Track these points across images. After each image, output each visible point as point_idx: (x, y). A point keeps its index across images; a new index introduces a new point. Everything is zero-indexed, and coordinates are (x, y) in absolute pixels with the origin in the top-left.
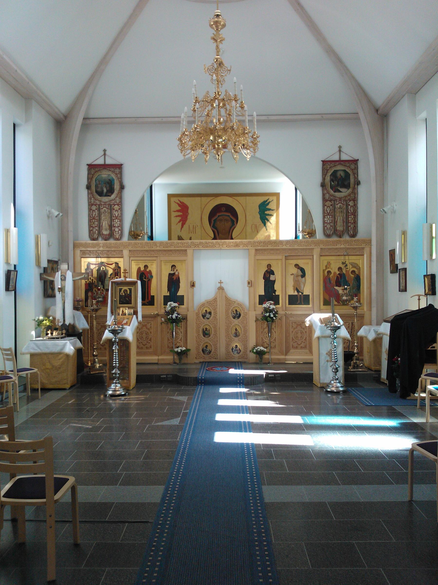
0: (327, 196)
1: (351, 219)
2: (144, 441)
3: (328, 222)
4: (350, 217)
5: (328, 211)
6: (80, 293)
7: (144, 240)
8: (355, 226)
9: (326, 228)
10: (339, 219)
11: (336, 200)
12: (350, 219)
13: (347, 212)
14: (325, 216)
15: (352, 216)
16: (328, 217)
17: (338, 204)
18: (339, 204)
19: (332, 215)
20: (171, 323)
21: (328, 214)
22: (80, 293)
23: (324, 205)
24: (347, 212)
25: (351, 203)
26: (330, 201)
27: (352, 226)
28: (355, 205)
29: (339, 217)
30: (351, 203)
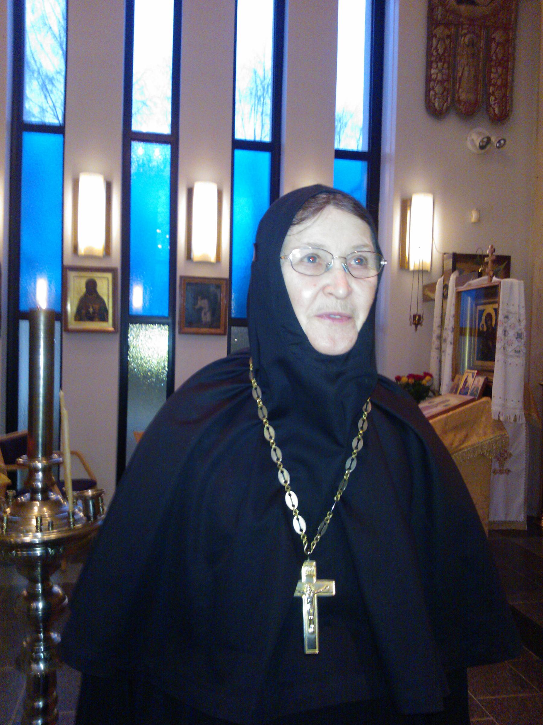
0: (439, 13)
1: (496, 76)
2: (5, 525)
3: (440, 77)
4: (493, 70)
5: (440, 52)
6: (224, 302)
7: (309, 648)
8: (505, 96)
9: (432, 93)
10: (466, 73)
11: (462, 24)
12: (492, 76)
13: (488, 58)
14: (432, 62)
15: (500, 70)
16: (440, 64)
17: (465, 35)
18: (468, 37)
19: (449, 62)
20: (497, 120)
21: (440, 59)
22: (224, 302)
23: (430, 36)
24: (488, 58)
25: (498, 36)
26: (447, 25)
27: (498, 93)
28: (508, 41)
29: (466, 68)
30: (498, 36)
